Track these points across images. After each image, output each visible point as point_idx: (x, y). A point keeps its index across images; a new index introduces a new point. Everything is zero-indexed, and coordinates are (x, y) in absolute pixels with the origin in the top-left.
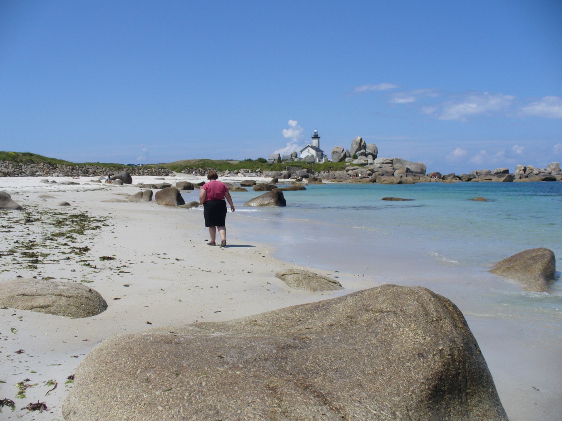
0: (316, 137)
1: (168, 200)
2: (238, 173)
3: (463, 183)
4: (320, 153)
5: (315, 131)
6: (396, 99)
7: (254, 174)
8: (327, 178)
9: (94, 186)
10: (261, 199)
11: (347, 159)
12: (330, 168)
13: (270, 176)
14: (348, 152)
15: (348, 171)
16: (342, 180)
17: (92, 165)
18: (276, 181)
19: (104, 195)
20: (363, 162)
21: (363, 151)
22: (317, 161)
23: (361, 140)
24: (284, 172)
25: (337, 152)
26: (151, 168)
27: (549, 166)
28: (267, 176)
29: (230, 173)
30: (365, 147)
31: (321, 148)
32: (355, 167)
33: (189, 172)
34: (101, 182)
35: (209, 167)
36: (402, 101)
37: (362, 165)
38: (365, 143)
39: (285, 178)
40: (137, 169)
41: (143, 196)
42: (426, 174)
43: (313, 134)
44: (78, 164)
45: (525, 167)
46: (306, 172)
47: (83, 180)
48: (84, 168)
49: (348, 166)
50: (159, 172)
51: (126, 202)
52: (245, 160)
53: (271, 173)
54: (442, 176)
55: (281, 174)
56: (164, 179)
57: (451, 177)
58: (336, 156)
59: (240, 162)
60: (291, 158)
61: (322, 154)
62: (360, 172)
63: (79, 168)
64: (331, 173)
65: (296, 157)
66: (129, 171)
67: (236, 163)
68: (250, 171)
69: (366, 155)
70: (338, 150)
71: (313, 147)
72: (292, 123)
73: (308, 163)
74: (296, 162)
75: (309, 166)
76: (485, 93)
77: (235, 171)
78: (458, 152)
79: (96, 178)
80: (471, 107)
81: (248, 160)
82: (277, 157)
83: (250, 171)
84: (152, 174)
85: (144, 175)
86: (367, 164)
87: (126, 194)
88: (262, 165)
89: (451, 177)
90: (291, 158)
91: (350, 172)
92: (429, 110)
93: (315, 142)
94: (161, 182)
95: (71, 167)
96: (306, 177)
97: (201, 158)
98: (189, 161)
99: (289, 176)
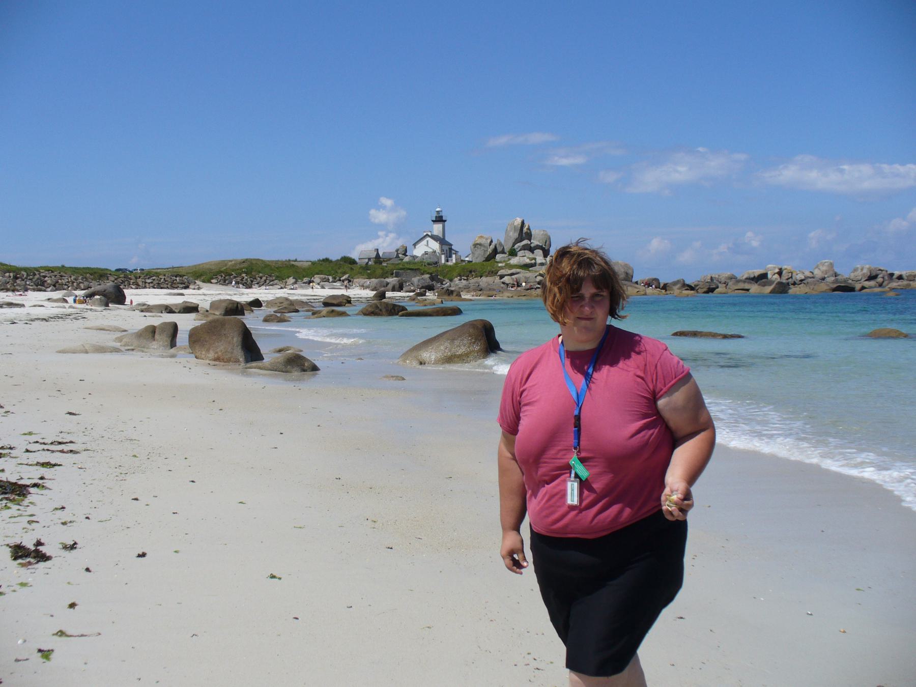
0: (439, 219)
1: (221, 347)
2: (310, 282)
3: (701, 297)
4: (446, 248)
5: (438, 209)
6: (556, 158)
7: (338, 284)
8: (467, 289)
9: (52, 309)
10: (447, 344)
11: (499, 257)
12: (471, 272)
13: (367, 287)
14: (501, 244)
15: (502, 277)
16: (494, 293)
17: (50, 270)
18: (382, 296)
19: (73, 333)
20: (528, 261)
21: (526, 242)
22: (443, 261)
23: (523, 223)
24: (392, 280)
25: (480, 245)
26: (157, 274)
27: (817, 267)
28: (363, 287)
29: (295, 283)
30: (529, 236)
31: (447, 239)
32: (514, 271)
33: (225, 282)
34: (66, 301)
35: (260, 272)
36: (565, 162)
37: (527, 267)
38: (529, 229)
39: (393, 290)
40: (132, 277)
41: (157, 336)
42: (634, 280)
43: (435, 214)
44: (25, 269)
45: (781, 269)
46: (428, 280)
47: (33, 297)
48: (37, 276)
49: (502, 268)
50: (173, 283)
51: (116, 350)
52: (319, 261)
53: (368, 282)
54: (662, 285)
55: (388, 284)
56: (182, 295)
57: (678, 286)
58: (479, 252)
59: (313, 263)
60: (397, 256)
61: (451, 249)
62: (523, 279)
63: (28, 275)
64: (473, 281)
65: (405, 254)
66: (119, 280)
67: (307, 264)
68: (331, 280)
69: (532, 250)
70: (483, 241)
71: (435, 238)
72: (388, 202)
73: (429, 264)
74: (407, 263)
75: (432, 269)
76: (700, 149)
77: (306, 280)
78: (655, 244)
79: (58, 295)
80: (680, 171)
81: (323, 260)
82: (374, 255)
83: (331, 280)
84: (159, 286)
85: (145, 287)
86: (534, 265)
87: (117, 329)
88: (352, 269)
89: (678, 286)
90: (397, 256)
91: (506, 279)
92: (610, 177)
93: (437, 229)
94: (179, 300)
95: (12, 275)
96: (431, 288)
97: (244, 257)
98: (224, 263)
99: (400, 288)
